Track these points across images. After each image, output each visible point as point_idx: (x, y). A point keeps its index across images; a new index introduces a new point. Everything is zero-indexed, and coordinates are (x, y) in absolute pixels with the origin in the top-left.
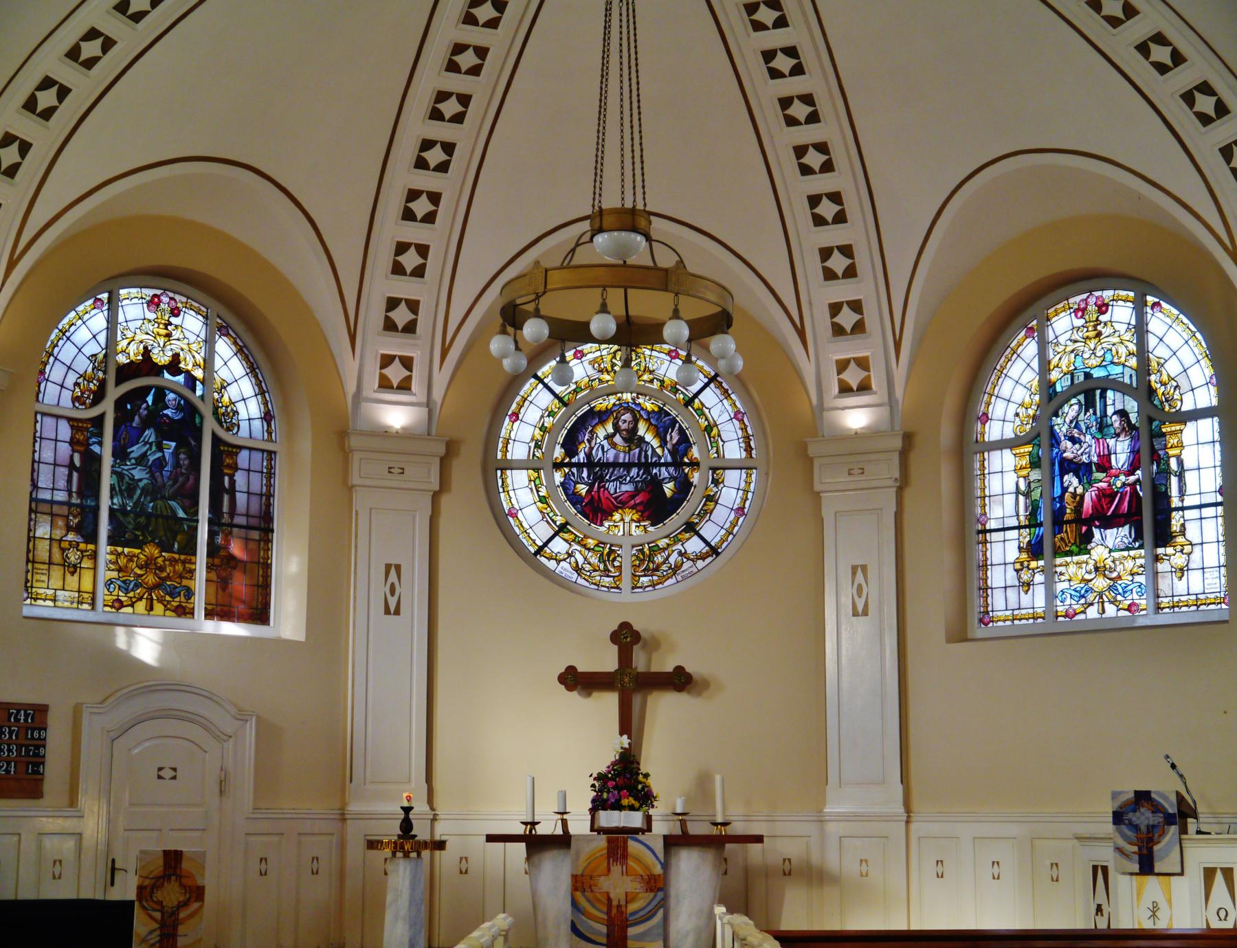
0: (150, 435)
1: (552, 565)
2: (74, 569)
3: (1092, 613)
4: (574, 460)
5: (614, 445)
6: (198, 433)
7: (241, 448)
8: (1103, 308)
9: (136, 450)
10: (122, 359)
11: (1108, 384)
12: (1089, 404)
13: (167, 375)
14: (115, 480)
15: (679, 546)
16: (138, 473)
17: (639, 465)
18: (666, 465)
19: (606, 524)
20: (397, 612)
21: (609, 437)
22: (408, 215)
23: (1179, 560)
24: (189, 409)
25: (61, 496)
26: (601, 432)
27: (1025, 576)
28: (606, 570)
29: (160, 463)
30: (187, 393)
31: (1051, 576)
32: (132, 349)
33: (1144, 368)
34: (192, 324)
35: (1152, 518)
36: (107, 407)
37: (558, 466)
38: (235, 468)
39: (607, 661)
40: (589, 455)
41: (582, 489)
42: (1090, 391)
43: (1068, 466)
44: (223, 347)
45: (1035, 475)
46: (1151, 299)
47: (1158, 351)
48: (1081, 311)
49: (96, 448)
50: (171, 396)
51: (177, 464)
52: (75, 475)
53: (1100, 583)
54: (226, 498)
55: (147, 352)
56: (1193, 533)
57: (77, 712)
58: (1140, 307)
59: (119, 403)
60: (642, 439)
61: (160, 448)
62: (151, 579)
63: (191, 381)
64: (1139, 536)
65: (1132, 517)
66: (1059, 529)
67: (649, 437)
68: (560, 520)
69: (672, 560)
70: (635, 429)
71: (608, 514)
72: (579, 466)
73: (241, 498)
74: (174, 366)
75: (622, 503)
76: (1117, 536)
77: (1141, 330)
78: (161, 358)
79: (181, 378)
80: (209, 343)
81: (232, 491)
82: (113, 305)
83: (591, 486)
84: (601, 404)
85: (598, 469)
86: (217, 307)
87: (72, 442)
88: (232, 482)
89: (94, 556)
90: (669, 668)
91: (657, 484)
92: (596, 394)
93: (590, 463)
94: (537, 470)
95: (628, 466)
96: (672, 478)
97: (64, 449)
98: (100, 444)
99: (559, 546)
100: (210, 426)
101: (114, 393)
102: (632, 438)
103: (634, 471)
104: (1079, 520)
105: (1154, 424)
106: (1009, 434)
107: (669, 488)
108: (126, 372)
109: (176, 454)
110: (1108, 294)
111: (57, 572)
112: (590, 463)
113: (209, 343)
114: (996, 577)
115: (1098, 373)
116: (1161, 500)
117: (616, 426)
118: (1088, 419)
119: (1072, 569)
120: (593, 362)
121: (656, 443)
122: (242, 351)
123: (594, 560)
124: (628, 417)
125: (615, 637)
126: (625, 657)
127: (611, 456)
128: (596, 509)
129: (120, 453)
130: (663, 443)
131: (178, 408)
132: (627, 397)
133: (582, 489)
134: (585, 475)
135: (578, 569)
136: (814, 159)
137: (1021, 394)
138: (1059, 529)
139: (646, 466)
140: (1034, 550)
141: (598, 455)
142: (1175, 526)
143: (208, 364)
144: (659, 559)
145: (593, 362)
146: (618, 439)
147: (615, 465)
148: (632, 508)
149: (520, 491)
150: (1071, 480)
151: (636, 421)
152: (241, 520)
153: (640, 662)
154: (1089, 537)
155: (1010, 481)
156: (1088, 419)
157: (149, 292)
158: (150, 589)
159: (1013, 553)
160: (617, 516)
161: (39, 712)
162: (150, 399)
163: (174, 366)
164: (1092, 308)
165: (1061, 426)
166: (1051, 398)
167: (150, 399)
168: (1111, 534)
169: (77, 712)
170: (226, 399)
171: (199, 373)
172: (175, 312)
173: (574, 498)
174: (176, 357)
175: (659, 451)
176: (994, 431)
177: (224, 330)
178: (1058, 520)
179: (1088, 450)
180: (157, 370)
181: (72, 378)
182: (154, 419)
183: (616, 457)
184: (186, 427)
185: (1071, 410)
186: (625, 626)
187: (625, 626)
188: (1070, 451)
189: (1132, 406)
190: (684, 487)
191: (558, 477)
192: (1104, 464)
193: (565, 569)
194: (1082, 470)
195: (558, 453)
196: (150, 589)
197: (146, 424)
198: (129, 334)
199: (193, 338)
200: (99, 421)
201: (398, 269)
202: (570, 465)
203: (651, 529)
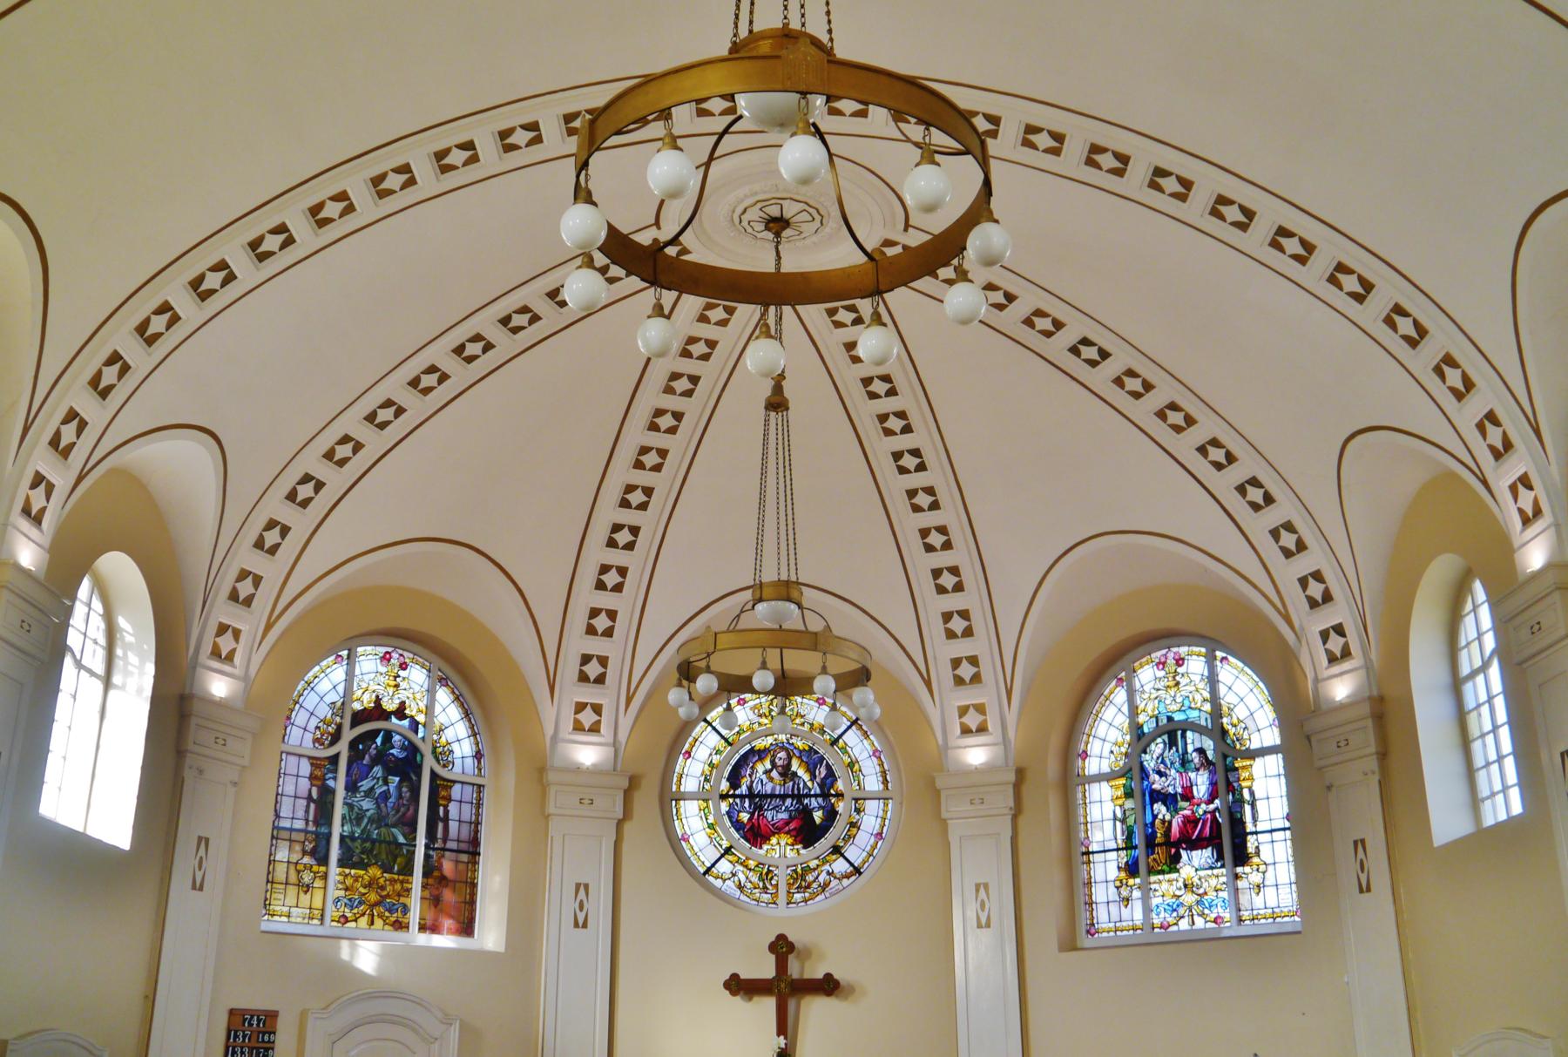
0: (378, 771)
1: (718, 883)
2: (308, 888)
3: (1184, 925)
4: (738, 792)
5: (771, 779)
6: (418, 769)
7: (454, 782)
8: (1180, 661)
9: (365, 785)
10: (357, 706)
11: (1187, 726)
12: (1172, 743)
13: (394, 720)
14: (346, 810)
15: (827, 867)
16: (367, 804)
17: (793, 796)
18: (816, 796)
19: (765, 847)
20: (585, 926)
21: (767, 772)
22: (600, 585)
23: (1256, 878)
24: (412, 749)
25: (299, 824)
26: (760, 768)
27: (1125, 892)
28: (765, 887)
29: (385, 796)
30: (411, 735)
31: (1146, 891)
32: (366, 698)
33: (1217, 713)
34: (417, 676)
35: (1229, 840)
36: (342, 747)
37: (723, 797)
38: (449, 799)
39: (766, 969)
40: (750, 788)
41: (745, 817)
42: (1173, 732)
43: (1157, 796)
44: (443, 696)
45: (1129, 804)
46: (1219, 654)
47: (1227, 698)
48: (1162, 664)
49: (331, 783)
50: (397, 738)
51: (400, 797)
52: (312, 806)
53: (1189, 899)
54: (440, 826)
55: (378, 700)
56: (1266, 854)
57: (303, 1015)
58: (1210, 659)
59: (353, 745)
60: (795, 774)
61: (386, 783)
62: (373, 897)
63: (415, 725)
64: (1220, 857)
65: (1212, 840)
66: (1153, 851)
67: (801, 772)
68: (725, 844)
69: (821, 879)
70: (789, 765)
71: (766, 839)
72: (742, 797)
73: (453, 826)
74: (400, 712)
75: (779, 829)
76: (1203, 856)
77: (1213, 680)
78: (390, 705)
79: (406, 723)
80: (431, 692)
81: (446, 820)
82: (351, 658)
83: (752, 814)
84: (760, 744)
85: (757, 800)
86: (434, 658)
87: (312, 777)
88: (447, 812)
89: (325, 877)
90: (820, 975)
91: (807, 813)
92: (756, 735)
93: (751, 795)
94: (706, 800)
95: (783, 797)
96: (820, 807)
97: (304, 784)
98: (335, 779)
99: (724, 866)
100: (429, 763)
101: (349, 735)
102: (787, 773)
103: (788, 802)
104: (1168, 843)
105: (1227, 763)
106: (1106, 769)
107: (818, 816)
108: (359, 718)
109: (399, 787)
110: (1183, 650)
111: (292, 890)
112: (751, 795)
113: (431, 692)
114: (1100, 894)
115: (1178, 717)
116: (1237, 825)
117: (774, 765)
118: (1172, 755)
119: (1165, 886)
120: (753, 708)
121: (806, 777)
122: (458, 699)
123: (755, 879)
124: (782, 754)
125: (773, 947)
126: (781, 965)
127: (768, 788)
128: (756, 834)
129: (352, 787)
130: (813, 777)
131: (403, 748)
132: (782, 737)
133: (745, 817)
134: (747, 804)
135: (740, 887)
136: (936, 539)
137: (1114, 735)
138: (1153, 851)
139: (799, 797)
140: (1132, 869)
141: (757, 788)
142: (1251, 848)
143: (429, 710)
144: (810, 878)
145: (753, 708)
146: (774, 774)
147: (773, 796)
148: (787, 833)
149: (692, 820)
150: (1160, 808)
151: (790, 758)
152: (452, 845)
153: (794, 970)
154: (1176, 859)
155: (1109, 809)
156: (1172, 755)
157: (382, 650)
158: (373, 906)
159: (1113, 873)
160: (774, 840)
161: (273, 1015)
162: (379, 740)
163: (400, 712)
164: (1171, 662)
165: (1150, 762)
166: (1140, 739)
167: (379, 740)
168: (1196, 854)
169: (303, 1015)
170: (443, 740)
171: (421, 718)
172: (403, 666)
173: (738, 825)
174: (403, 705)
175: (809, 784)
176: (1092, 766)
177: (444, 681)
178: (1150, 843)
179: (1172, 783)
180: (385, 715)
181: (314, 722)
182: (381, 758)
183: (773, 789)
184: (408, 766)
185: (1157, 748)
186: (781, 938)
187: (781, 938)
188: (1158, 783)
189: (1209, 745)
190: (831, 815)
191: (724, 807)
192: (1188, 795)
193: (730, 887)
194: (1169, 800)
195: (724, 786)
196: (373, 906)
197: (376, 761)
198: (364, 685)
199: (417, 688)
200: (334, 760)
201: (591, 631)
202: (734, 796)
203: (803, 851)
